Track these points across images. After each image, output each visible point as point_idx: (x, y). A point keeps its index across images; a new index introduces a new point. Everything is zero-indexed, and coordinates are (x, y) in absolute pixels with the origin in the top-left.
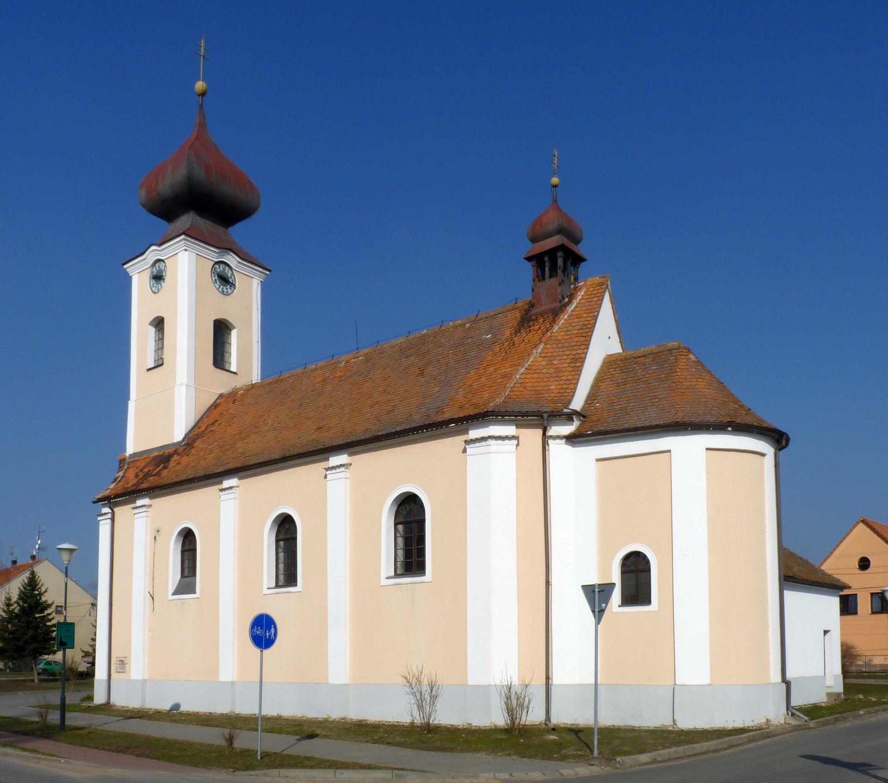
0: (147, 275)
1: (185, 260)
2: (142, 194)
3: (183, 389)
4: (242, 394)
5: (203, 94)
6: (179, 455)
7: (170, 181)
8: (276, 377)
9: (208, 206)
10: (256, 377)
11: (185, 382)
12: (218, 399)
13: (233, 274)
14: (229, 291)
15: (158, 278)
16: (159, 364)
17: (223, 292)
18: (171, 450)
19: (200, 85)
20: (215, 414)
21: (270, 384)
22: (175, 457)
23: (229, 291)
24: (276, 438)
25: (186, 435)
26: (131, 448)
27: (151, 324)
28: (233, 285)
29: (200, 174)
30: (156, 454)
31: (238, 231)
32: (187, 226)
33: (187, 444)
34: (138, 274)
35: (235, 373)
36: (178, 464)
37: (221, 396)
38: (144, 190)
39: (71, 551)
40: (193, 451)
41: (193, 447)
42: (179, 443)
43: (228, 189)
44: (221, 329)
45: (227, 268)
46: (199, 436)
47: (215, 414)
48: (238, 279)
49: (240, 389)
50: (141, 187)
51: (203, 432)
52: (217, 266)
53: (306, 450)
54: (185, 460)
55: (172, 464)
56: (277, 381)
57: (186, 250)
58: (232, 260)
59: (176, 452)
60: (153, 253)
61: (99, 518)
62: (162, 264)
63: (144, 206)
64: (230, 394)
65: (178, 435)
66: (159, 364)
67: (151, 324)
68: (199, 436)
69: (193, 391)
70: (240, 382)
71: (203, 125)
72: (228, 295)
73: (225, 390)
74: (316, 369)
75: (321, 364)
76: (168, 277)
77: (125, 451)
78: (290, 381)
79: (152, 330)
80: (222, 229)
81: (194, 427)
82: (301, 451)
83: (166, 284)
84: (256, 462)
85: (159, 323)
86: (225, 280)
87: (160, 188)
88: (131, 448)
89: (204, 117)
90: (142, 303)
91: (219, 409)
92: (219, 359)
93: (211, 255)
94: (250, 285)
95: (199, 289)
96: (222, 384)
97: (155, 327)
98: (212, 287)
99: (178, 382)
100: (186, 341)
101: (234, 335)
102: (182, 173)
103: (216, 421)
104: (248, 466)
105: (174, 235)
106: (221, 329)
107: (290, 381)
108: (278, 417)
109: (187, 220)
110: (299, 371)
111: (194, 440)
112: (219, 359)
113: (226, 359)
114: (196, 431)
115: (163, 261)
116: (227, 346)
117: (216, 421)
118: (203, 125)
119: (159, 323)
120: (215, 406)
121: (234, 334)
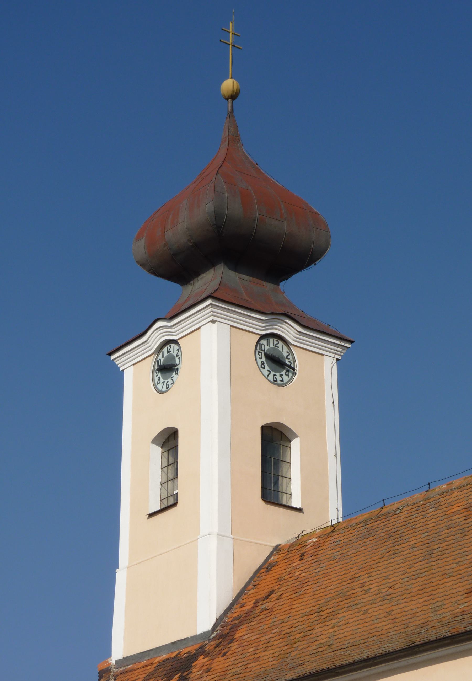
0: (149, 366)
1: (213, 339)
2: (140, 248)
3: (213, 543)
4: (314, 544)
5: (234, 96)
6: (206, 655)
7: (182, 227)
8: (375, 510)
9: (247, 255)
10: (334, 514)
11: (216, 530)
12: (271, 554)
13: (290, 352)
14: (286, 379)
15: (167, 368)
16: (170, 504)
17: (275, 382)
18: (192, 648)
19: (228, 85)
20: (268, 581)
21: (365, 523)
22: (201, 660)
23: (286, 379)
24: (390, 613)
25: (219, 620)
26: (118, 651)
27: (154, 441)
28: (291, 369)
29: (234, 208)
30: (165, 656)
31: (294, 287)
32: (215, 284)
33: (222, 636)
34: (135, 368)
35: (299, 510)
36: (208, 671)
37: (277, 549)
38: (142, 244)
39: (348, 348)
40: (234, 646)
41: (232, 641)
42: (206, 635)
43: (278, 225)
44: (274, 440)
45: (281, 344)
46: (242, 620)
47: (268, 581)
48: (300, 360)
49: (310, 535)
50: (138, 238)
51: (249, 613)
52: (264, 342)
53: (454, 632)
54: (219, 664)
55: (195, 672)
56: (378, 517)
57: (213, 322)
58: (289, 330)
59: (201, 651)
60: (156, 336)
61: (112, 357)
62: (173, 348)
63: (142, 265)
64: (292, 545)
65: (204, 621)
66: (170, 504)
67: (154, 441)
68: (242, 620)
69: (229, 543)
70: (309, 524)
71: (234, 139)
72: (283, 384)
73: (284, 537)
74: (449, 491)
75: (457, 482)
76: (183, 368)
77: (109, 654)
78: (403, 515)
79: (157, 450)
80: (270, 286)
81: (232, 605)
82: (445, 632)
83: (180, 379)
84: (357, 658)
85: (169, 440)
86: (277, 363)
87: (169, 234)
88: (118, 651)
89: (236, 127)
90: (142, 406)
91: (275, 573)
92: (272, 489)
93: (256, 325)
94: (319, 369)
95: (235, 380)
96: (278, 529)
97: (162, 447)
98: (256, 376)
99: (203, 530)
100: (217, 463)
101: (295, 448)
102: (205, 209)
103: (272, 592)
104: (342, 667)
105: (190, 302)
106: (274, 440)
107: (403, 515)
108: (387, 577)
109: (210, 278)
110: (418, 496)
111: (234, 628)
112: (272, 489)
113: (283, 488)
114: (237, 612)
115: (175, 342)
116: (284, 467)
117: (272, 592)
118: (234, 139)
119: (169, 440)
120: (267, 567)
121: (295, 446)
